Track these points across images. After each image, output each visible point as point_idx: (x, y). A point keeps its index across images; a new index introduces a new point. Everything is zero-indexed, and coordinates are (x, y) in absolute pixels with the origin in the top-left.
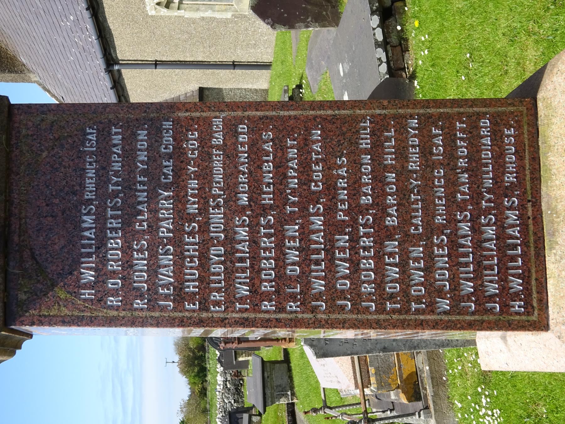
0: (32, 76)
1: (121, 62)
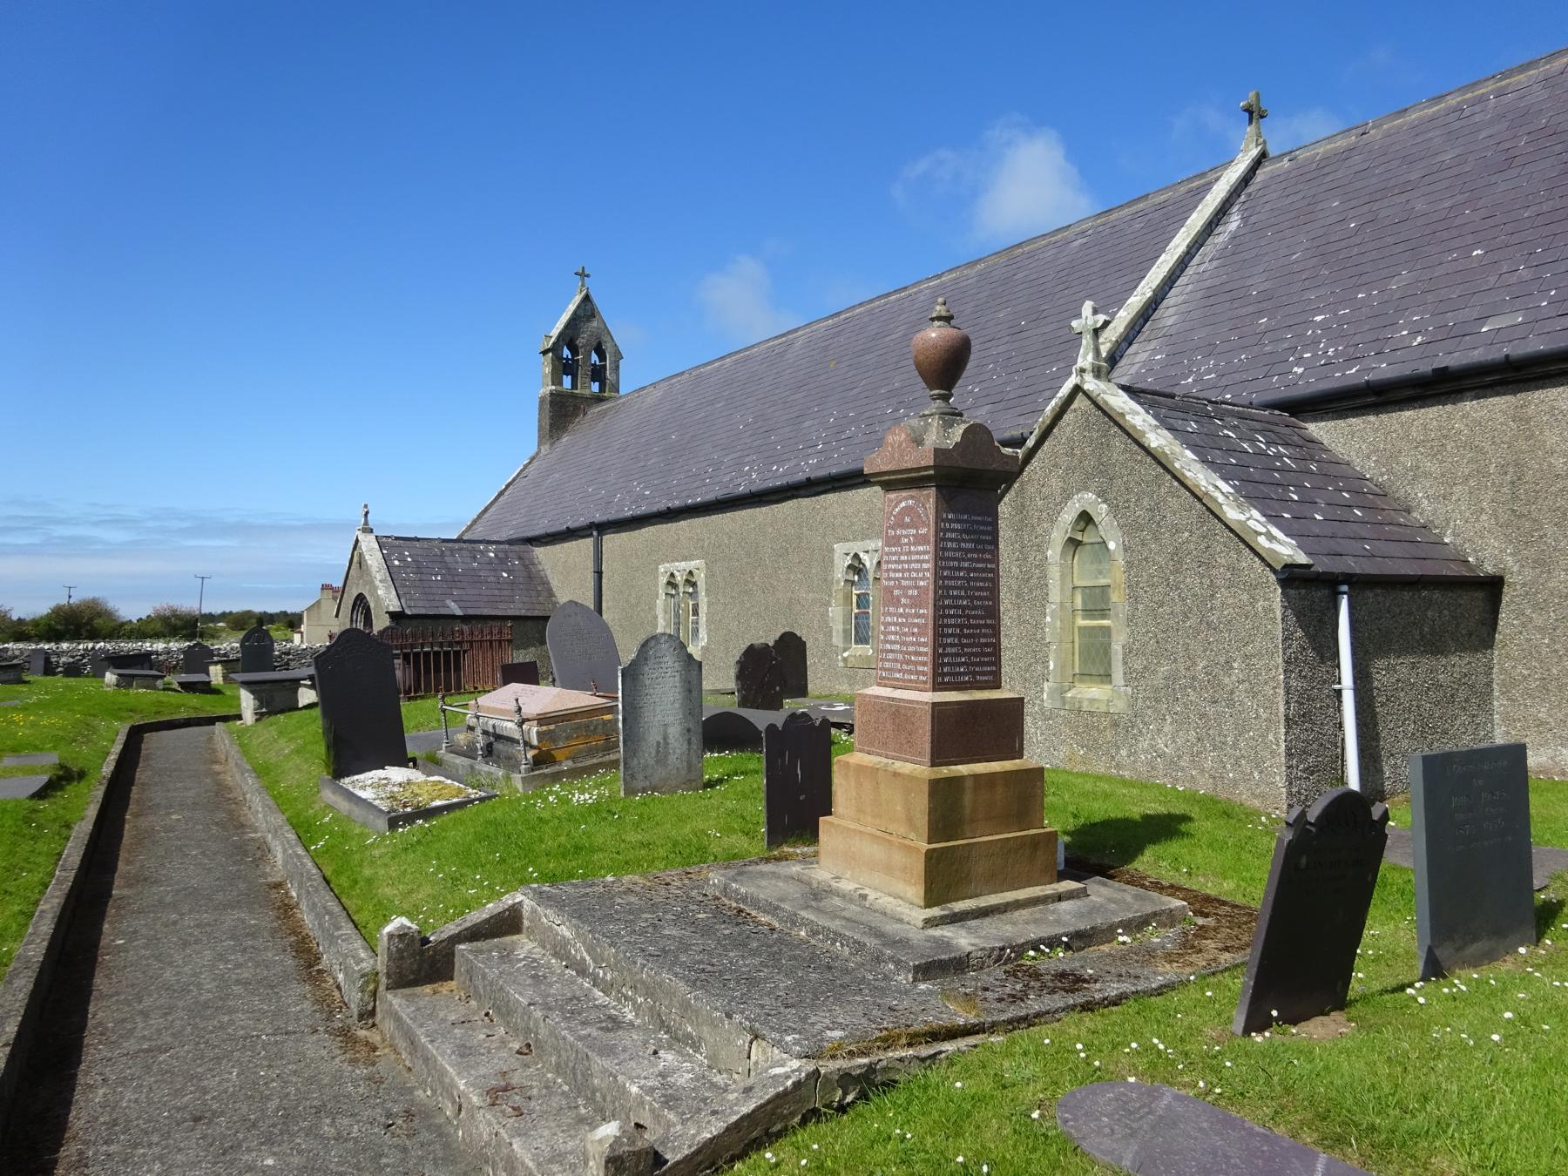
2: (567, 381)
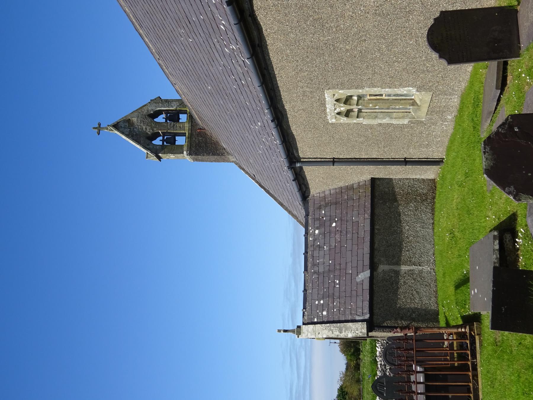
0: (230, 157)
1: (302, 160)
2: (181, 141)
